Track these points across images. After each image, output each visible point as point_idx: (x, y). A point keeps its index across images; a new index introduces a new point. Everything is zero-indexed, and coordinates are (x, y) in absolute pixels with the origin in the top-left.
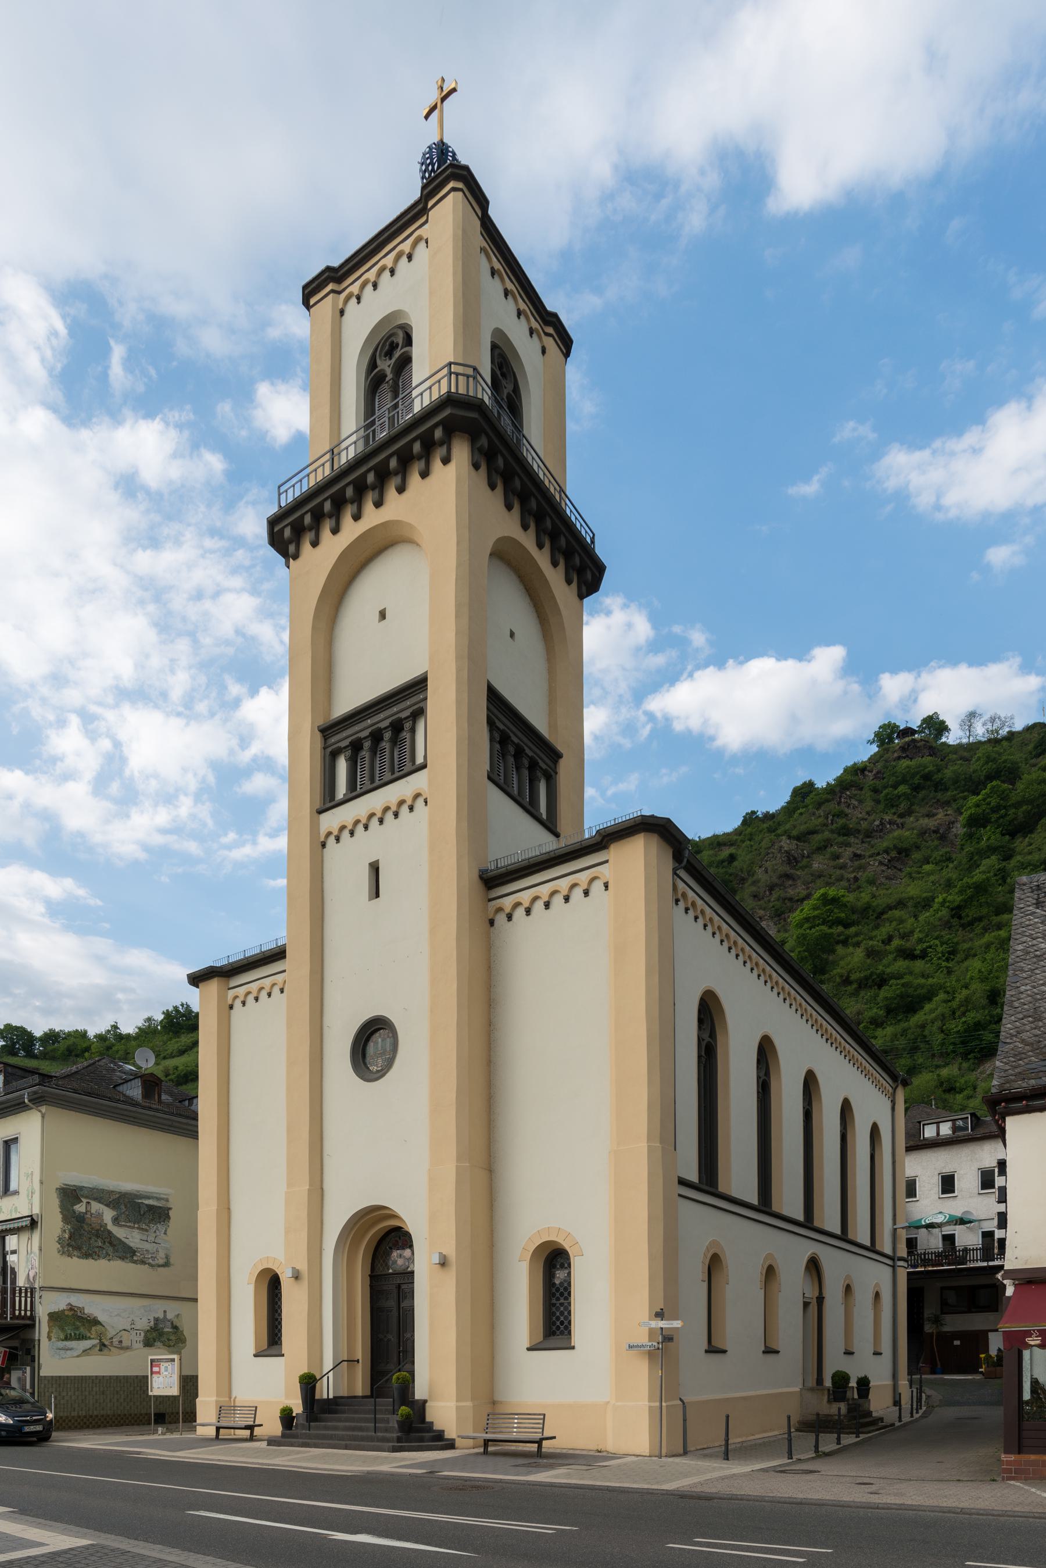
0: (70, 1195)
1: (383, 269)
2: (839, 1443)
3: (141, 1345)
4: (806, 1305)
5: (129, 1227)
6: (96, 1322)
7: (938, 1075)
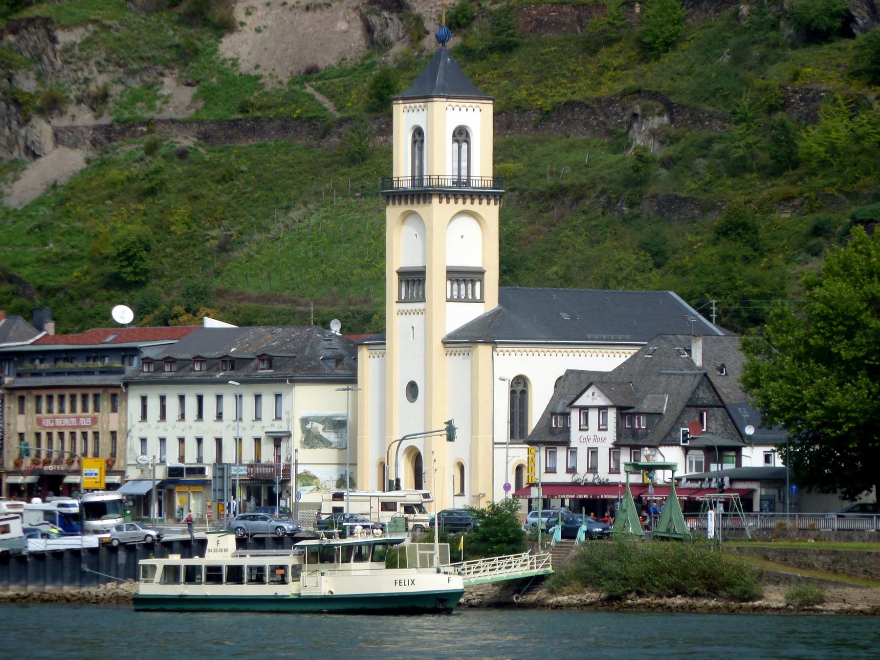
6: (315, 478)
7: (834, 235)
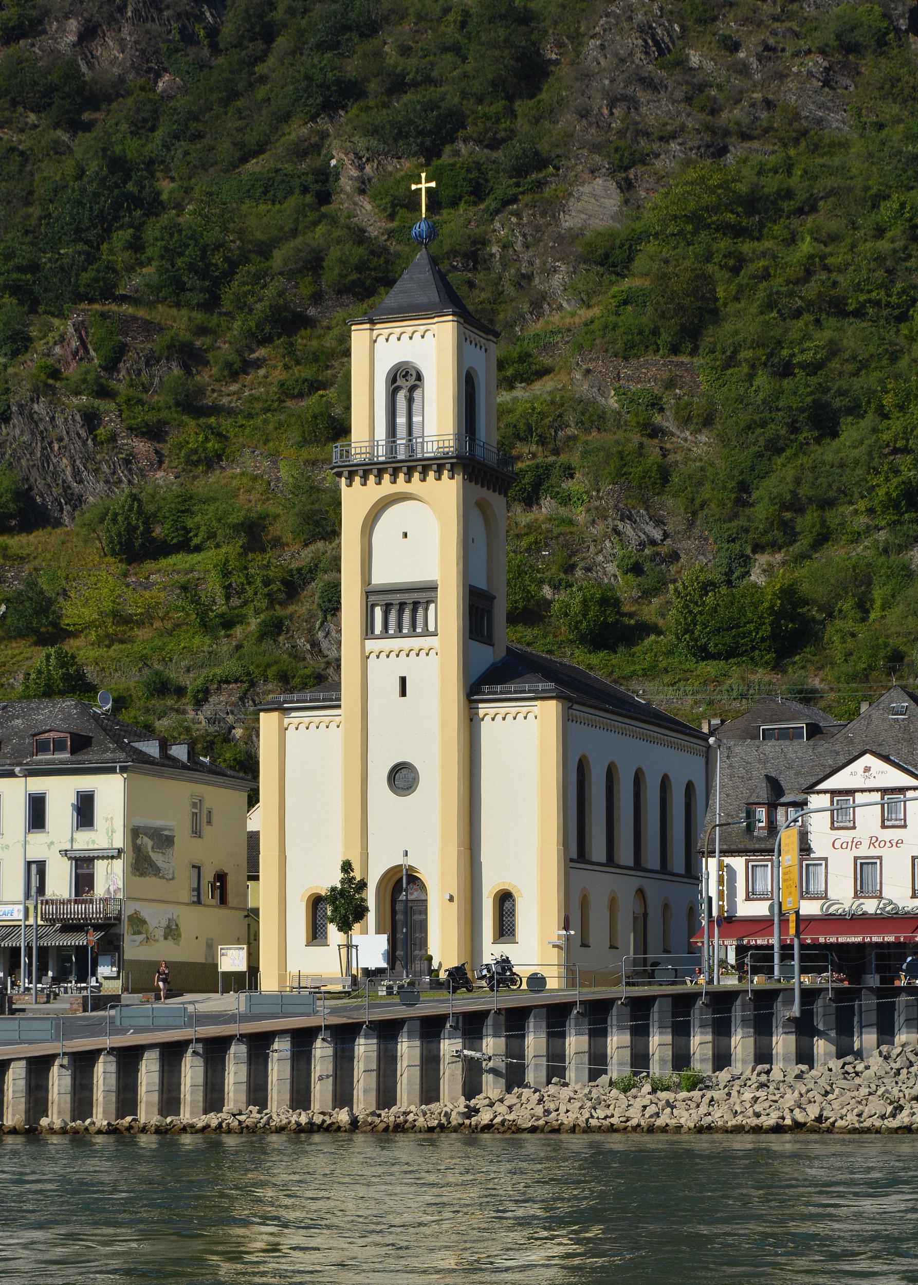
0: (134, 833)
4: (635, 919)
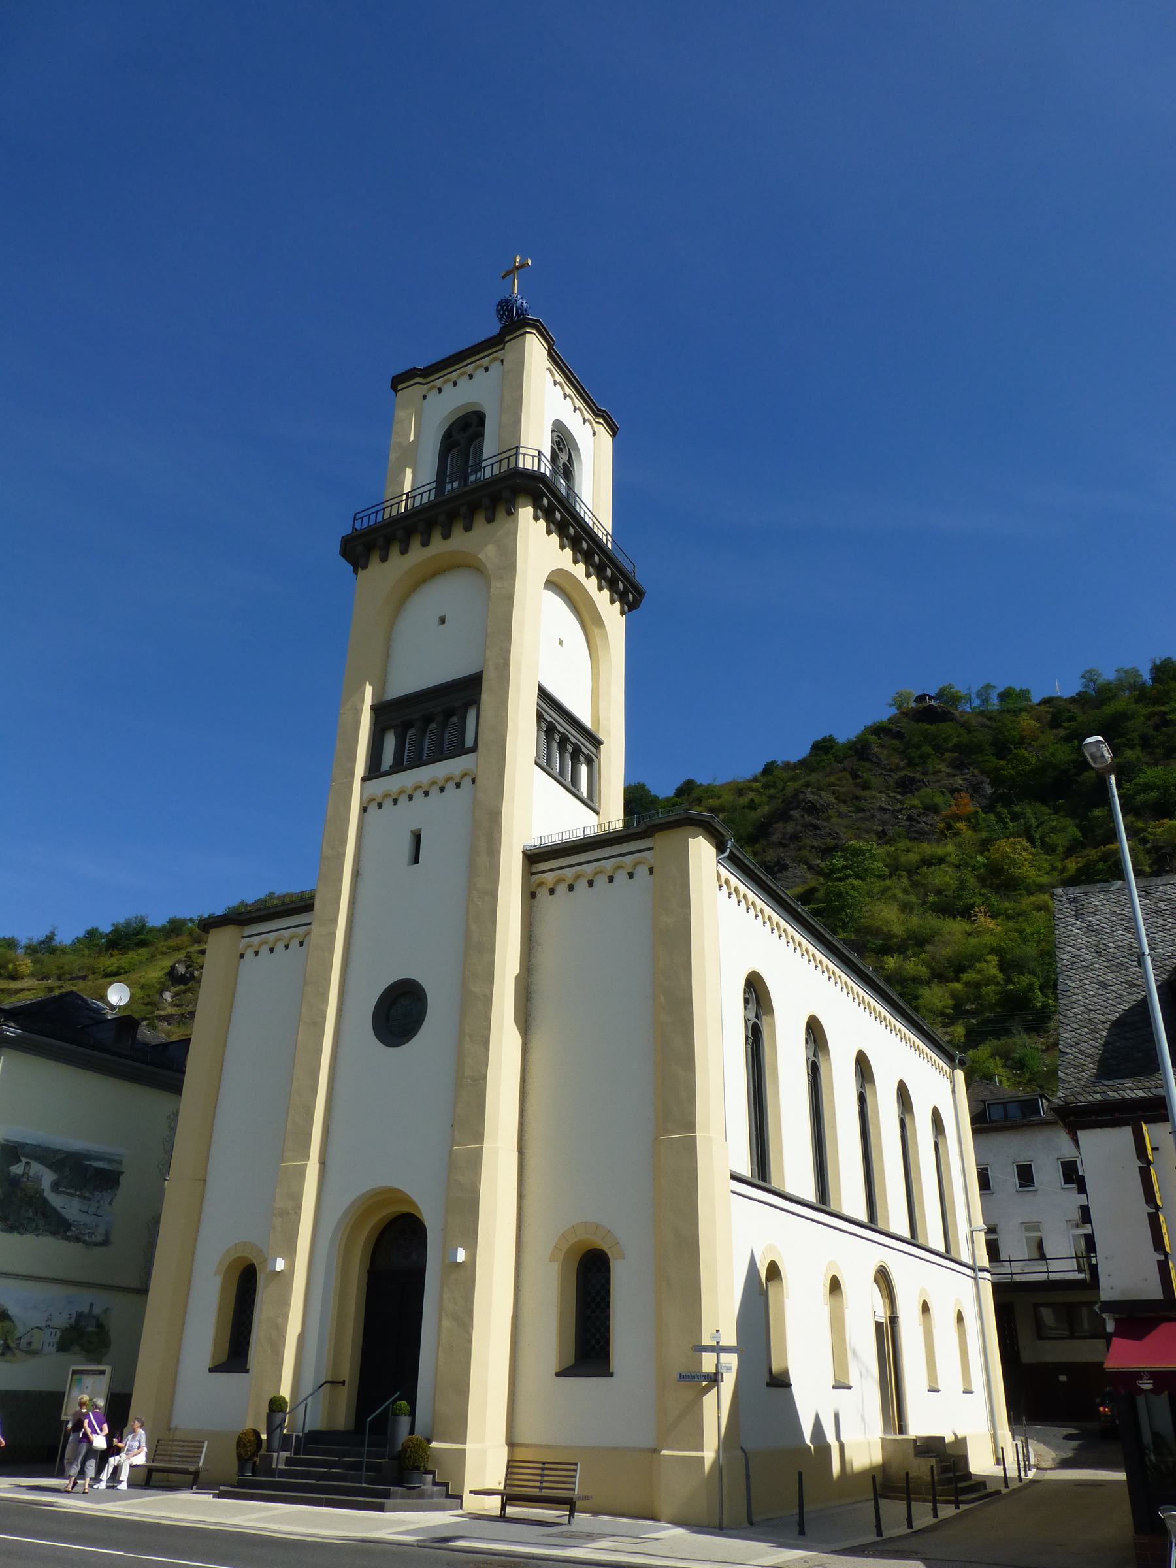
1: (465, 373)
2: (935, 1516)
3: (53, 1349)
5: (69, 1194)
